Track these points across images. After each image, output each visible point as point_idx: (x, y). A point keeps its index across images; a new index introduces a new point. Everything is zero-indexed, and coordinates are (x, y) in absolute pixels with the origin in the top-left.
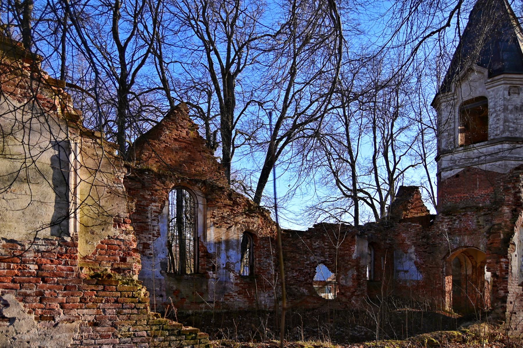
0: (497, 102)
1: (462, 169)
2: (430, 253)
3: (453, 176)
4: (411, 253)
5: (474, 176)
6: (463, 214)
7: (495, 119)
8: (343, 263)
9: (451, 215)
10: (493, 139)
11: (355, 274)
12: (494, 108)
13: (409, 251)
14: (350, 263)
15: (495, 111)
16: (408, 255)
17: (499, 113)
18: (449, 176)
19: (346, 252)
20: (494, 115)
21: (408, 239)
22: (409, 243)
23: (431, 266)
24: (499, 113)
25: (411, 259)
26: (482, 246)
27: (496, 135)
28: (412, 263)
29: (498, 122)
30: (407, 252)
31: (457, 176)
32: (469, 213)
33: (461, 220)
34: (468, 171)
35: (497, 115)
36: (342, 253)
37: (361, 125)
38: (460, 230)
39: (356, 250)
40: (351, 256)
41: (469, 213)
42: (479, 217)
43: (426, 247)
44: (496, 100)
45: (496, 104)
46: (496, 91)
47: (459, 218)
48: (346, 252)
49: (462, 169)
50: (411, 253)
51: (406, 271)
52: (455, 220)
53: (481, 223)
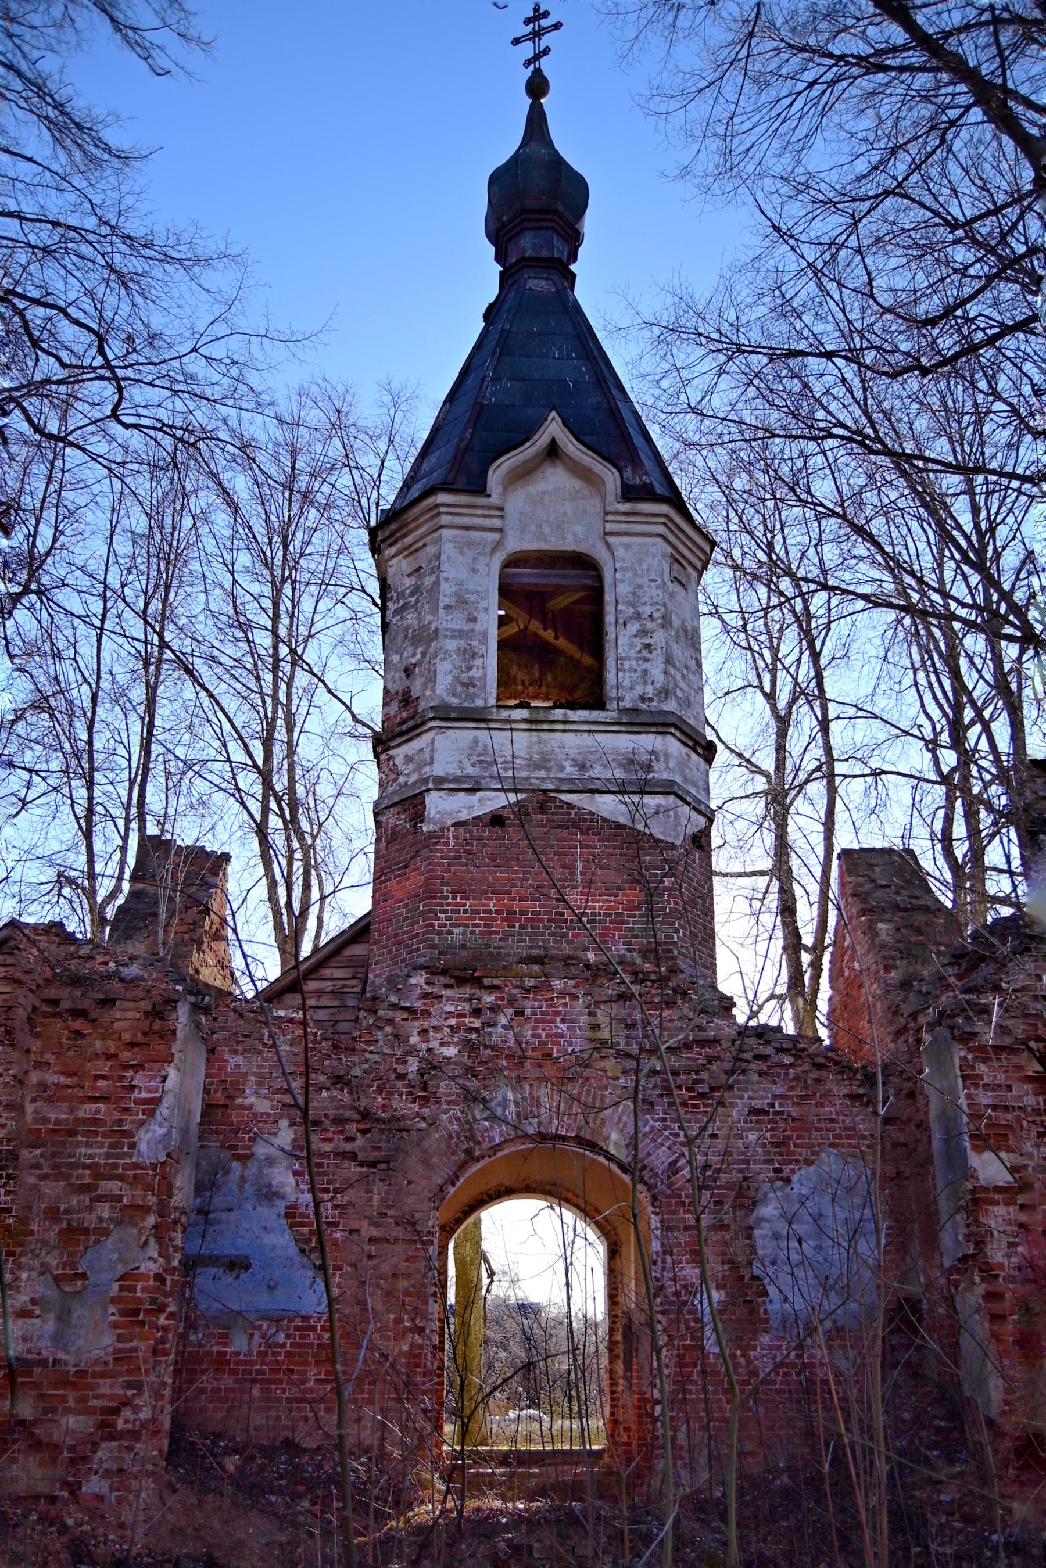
0: (640, 587)
1: (512, 797)
2: (373, 1164)
3: (478, 818)
4: (270, 1161)
5: (564, 833)
6: (530, 983)
7: (638, 642)
8: (51, 1189)
9: (477, 982)
10: (635, 710)
11: (150, 1268)
12: (632, 604)
13: (261, 1150)
14: (113, 1186)
15: (638, 616)
16: (252, 1168)
17: (650, 625)
18: (464, 816)
19: (86, 1110)
20: (633, 628)
21: (260, 1084)
22: (263, 1106)
23: (375, 1233)
24: (650, 625)
25: (269, 1194)
26: (614, 1136)
27: (643, 699)
28: (272, 1214)
29: (645, 653)
30: (249, 1157)
31: (496, 819)
32: (557, 984)
33: (519, 1013)
34: (542, 807)
35: (643, 632)
36: (57, 1113)
37: (57, 507)
38: (518, 1059)
39: (168, 1101)
40: (123, 1137)
41: (557, 984)
42: (597, 1003)
43: (352, 1128)
44: (639, 581)
45: (639, 592)
46: (635, 548)
47: (512, 1002)
48: (86, 1110)
49: (512, 797)
50: (270, 1161)
51: (238, 1265)
52: (495, 1009)
53: (605, 1034)
